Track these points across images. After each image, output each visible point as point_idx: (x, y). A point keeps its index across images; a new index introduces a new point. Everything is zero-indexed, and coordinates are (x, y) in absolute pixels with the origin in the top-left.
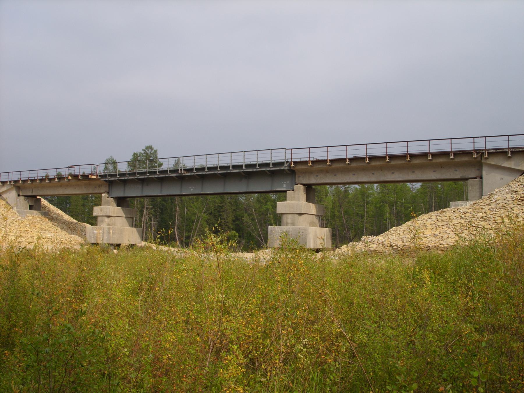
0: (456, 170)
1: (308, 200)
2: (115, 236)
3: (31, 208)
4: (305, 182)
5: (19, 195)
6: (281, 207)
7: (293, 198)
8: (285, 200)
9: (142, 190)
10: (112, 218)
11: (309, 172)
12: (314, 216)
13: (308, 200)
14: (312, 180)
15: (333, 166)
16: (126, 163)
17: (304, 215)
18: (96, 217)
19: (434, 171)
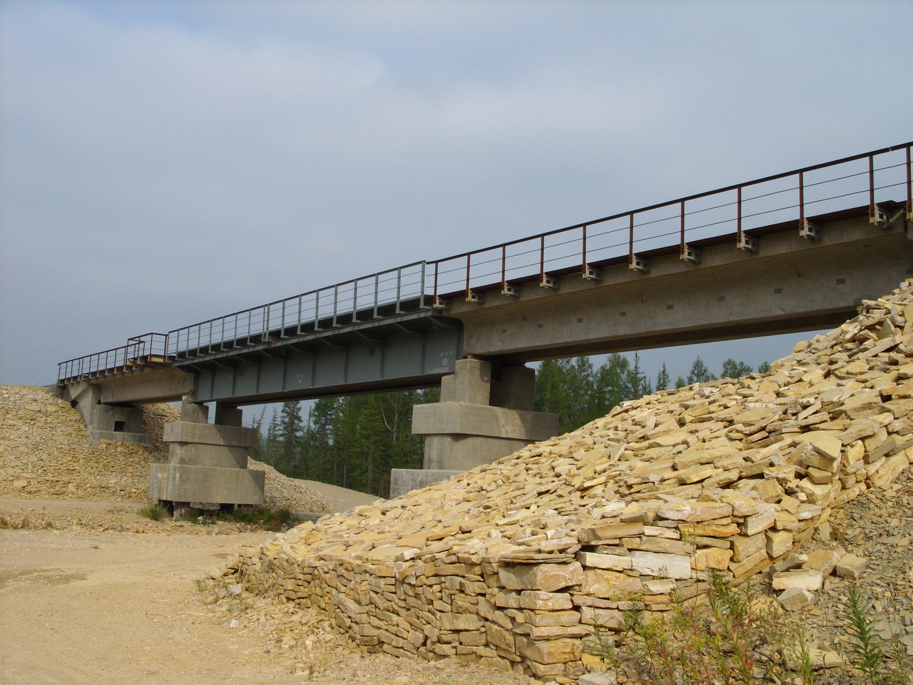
0: (841, 281)
1: (496, 399)
2: (188, 486)
3: (119, 426)
4: (481, 349)
5: (99, 403)
6: (424, 417)
7: (453, 396)
8: (435, 399)
9: (346, 372)
10: (190, 446)
11: (486, 322)
12: (226, 449)
13: (496, 399)
14: (498, 345)
15: (522, 299)
16: (905, 198)
17: (470, 441)
18: (167, 444)
19: (778, 291)
